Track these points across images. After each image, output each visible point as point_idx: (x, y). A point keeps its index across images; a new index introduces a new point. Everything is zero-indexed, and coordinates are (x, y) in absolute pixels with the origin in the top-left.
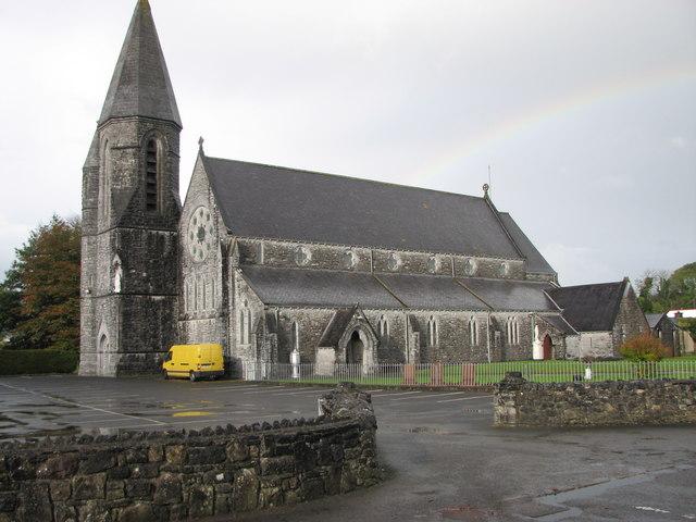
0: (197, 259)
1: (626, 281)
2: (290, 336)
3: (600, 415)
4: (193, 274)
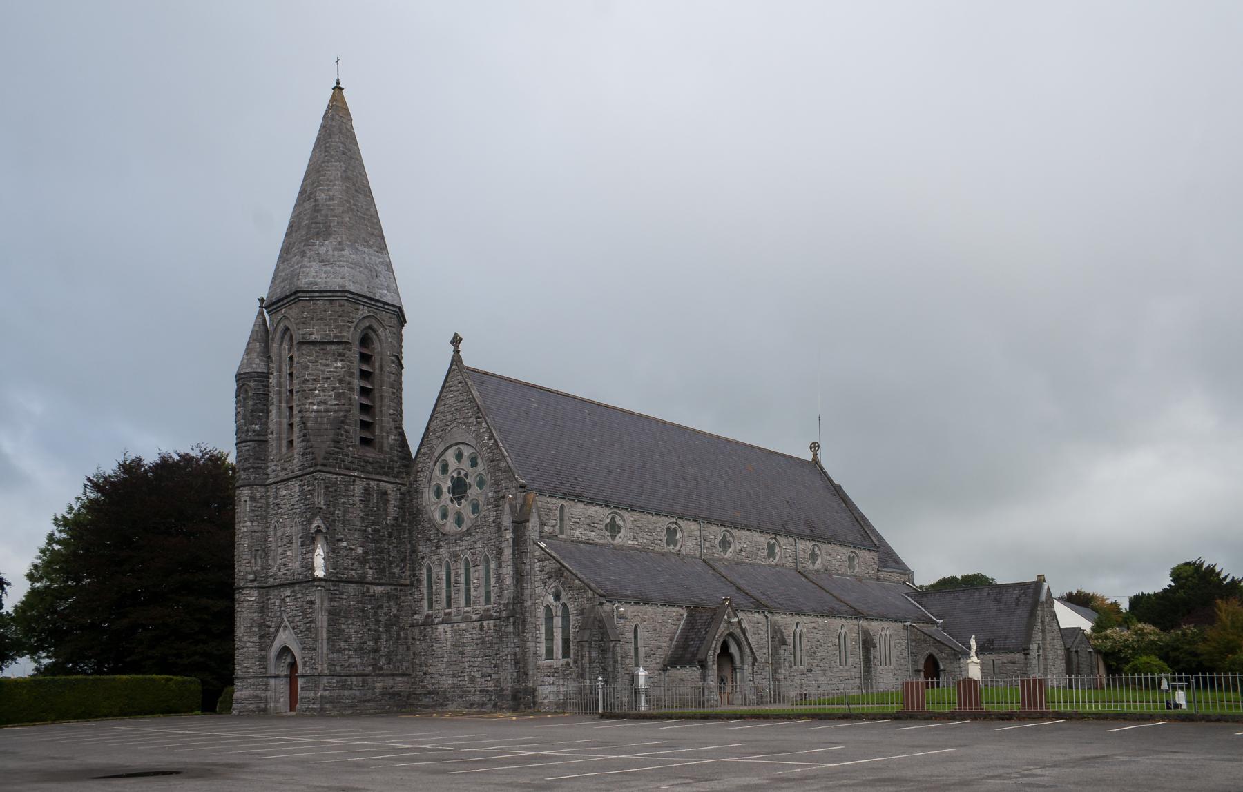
0: (450, 526)
1: (1041, 580)
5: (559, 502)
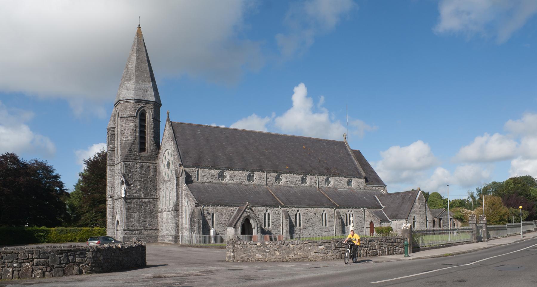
0: (166, 179)
2: (295, 224)
3: (273, 257)
4: (164, 187)
5: (197, 169)
